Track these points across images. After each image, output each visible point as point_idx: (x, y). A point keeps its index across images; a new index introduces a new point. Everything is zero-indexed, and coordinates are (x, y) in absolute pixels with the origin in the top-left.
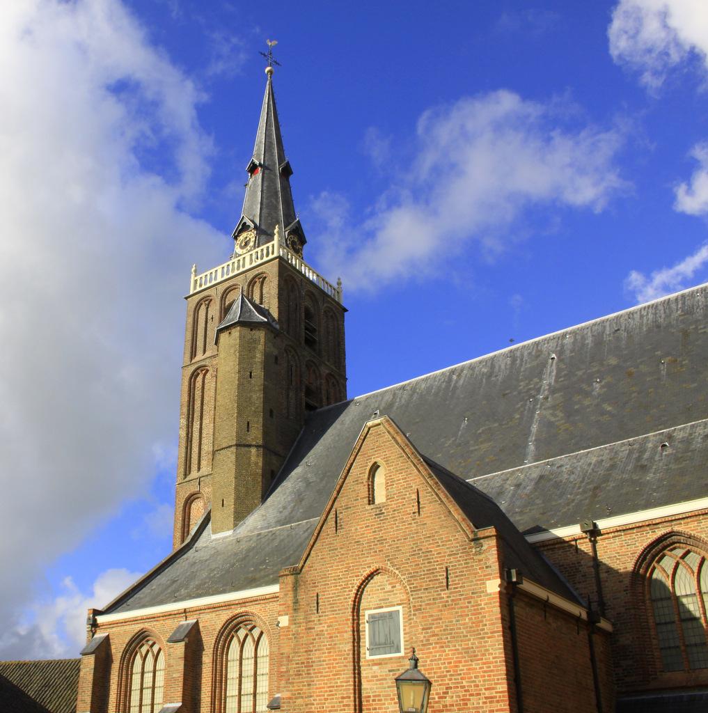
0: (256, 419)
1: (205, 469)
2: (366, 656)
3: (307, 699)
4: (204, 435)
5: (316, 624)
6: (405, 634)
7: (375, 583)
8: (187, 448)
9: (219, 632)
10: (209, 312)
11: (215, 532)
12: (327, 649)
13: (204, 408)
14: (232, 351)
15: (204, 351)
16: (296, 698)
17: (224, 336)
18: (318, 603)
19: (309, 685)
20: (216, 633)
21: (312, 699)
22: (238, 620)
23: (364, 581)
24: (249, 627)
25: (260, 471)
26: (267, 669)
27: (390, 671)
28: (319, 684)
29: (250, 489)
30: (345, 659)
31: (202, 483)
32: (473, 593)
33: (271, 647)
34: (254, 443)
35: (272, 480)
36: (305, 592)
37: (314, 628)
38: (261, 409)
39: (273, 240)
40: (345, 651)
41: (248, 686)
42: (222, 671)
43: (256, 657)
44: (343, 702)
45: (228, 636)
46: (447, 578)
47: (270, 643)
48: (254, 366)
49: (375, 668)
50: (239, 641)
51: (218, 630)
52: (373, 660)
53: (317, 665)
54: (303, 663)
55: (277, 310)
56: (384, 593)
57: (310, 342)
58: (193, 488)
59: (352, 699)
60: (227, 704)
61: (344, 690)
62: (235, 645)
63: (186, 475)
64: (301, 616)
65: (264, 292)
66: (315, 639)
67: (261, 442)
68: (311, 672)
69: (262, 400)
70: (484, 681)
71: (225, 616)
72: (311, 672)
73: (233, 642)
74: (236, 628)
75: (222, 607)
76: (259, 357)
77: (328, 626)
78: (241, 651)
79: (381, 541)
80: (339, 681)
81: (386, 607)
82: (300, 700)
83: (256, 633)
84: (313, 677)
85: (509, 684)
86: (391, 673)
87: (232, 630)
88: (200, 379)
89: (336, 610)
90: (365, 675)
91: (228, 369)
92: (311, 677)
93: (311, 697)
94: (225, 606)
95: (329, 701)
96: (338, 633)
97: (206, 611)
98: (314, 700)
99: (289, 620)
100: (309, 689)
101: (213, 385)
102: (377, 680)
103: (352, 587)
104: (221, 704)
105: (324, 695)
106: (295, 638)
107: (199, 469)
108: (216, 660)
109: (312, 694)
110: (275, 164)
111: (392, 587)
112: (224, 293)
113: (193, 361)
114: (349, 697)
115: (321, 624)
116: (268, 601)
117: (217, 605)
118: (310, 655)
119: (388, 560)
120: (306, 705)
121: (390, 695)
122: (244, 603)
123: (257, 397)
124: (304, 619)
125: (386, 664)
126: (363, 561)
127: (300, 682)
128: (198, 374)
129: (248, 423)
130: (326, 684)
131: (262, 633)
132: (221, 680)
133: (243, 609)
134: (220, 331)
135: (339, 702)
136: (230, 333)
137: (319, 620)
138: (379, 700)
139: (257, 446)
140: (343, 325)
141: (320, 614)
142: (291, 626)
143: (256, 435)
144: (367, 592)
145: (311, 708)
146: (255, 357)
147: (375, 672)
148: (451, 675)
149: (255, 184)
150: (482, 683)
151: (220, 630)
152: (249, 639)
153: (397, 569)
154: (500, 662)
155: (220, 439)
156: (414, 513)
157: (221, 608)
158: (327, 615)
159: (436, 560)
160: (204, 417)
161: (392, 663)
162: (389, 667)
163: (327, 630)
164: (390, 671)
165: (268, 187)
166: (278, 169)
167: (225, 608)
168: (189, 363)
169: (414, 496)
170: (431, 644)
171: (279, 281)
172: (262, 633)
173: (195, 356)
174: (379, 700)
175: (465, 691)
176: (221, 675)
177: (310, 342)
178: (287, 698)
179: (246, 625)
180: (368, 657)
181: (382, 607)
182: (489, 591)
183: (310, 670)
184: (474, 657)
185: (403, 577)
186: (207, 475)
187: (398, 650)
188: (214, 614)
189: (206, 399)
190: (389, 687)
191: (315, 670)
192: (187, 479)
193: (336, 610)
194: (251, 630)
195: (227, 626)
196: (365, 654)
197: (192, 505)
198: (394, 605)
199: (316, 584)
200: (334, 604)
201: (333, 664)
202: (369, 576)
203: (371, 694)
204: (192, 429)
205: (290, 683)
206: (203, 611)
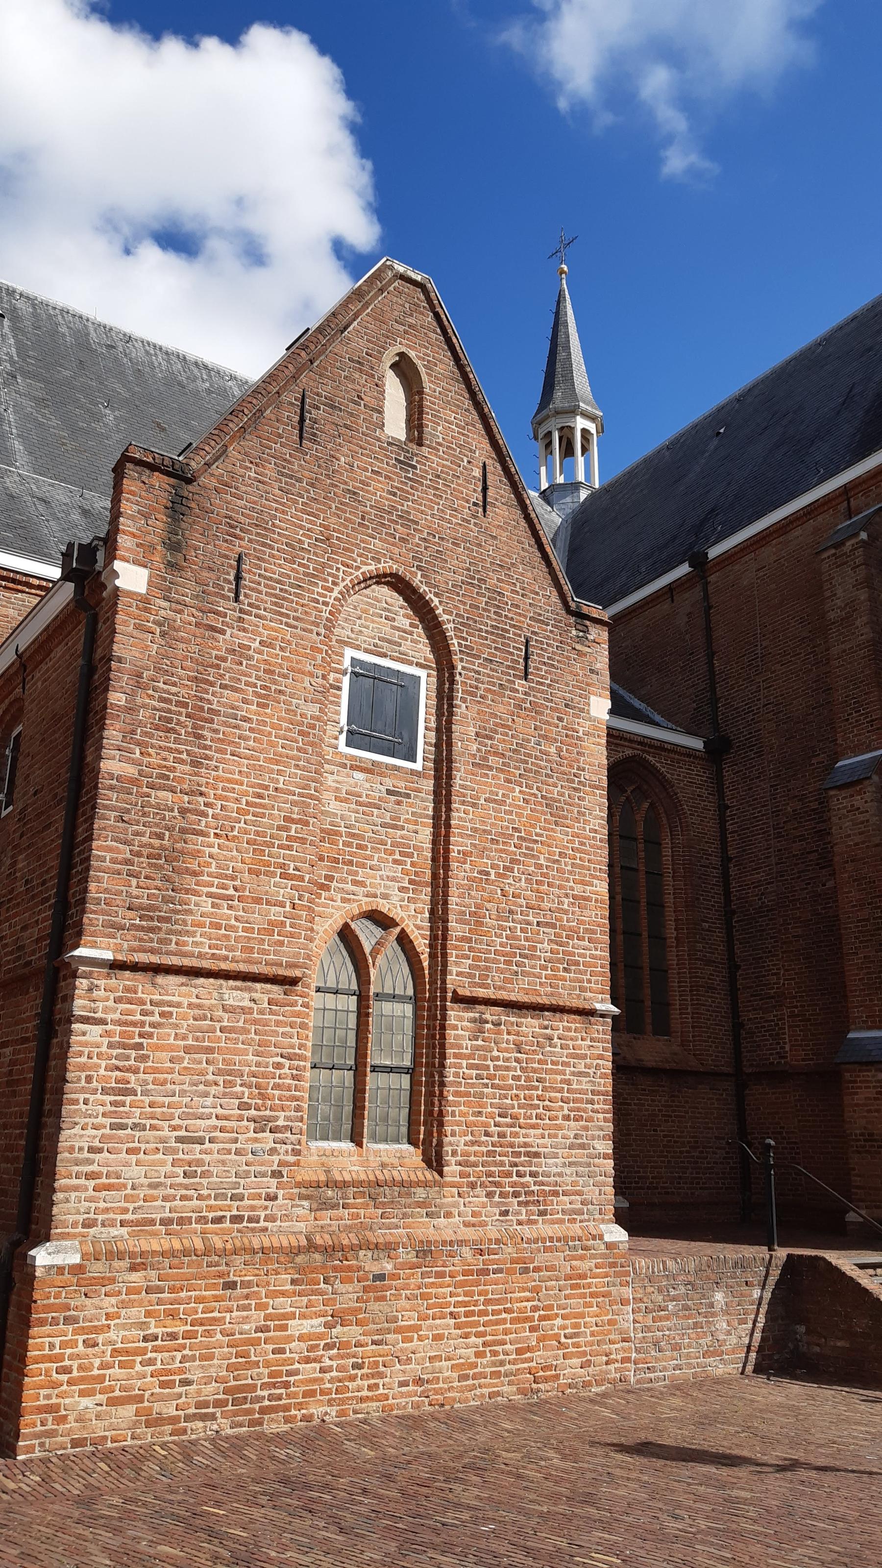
19: (195, 764)
32: (567, 706)
44: (288, 829)
46: (526, 659)
49: (359, 776)
53: (225, 724)
54: (185, 705)
64: (188, 591)
70: (573, 865)
81: (366, 651)
82: (162, 794)
84: (210, 748)
85: (24, 1347)
86: (393, 798)
102: (359, 804)
126: (362, 541)
135: (279, 828)
138: (360, 847)
148: (520, 838)
150: (569, 868)
153: (436, 595)
154: (79, 1080)
156: (475, 504)
159: (510, 615)
162: (389, 783)
164: (389, 792)
169: (477, 473)
170: (490, 768)
174: (360, 847)
175: (542, 875)
181: (384, 656)
182: (594, 713)
183: (202, 728)
184: (559, 819)
187: (412, 758)
191: (216, 731)
193: (288, 616)
198: (410, 663)
203: (343, 829)
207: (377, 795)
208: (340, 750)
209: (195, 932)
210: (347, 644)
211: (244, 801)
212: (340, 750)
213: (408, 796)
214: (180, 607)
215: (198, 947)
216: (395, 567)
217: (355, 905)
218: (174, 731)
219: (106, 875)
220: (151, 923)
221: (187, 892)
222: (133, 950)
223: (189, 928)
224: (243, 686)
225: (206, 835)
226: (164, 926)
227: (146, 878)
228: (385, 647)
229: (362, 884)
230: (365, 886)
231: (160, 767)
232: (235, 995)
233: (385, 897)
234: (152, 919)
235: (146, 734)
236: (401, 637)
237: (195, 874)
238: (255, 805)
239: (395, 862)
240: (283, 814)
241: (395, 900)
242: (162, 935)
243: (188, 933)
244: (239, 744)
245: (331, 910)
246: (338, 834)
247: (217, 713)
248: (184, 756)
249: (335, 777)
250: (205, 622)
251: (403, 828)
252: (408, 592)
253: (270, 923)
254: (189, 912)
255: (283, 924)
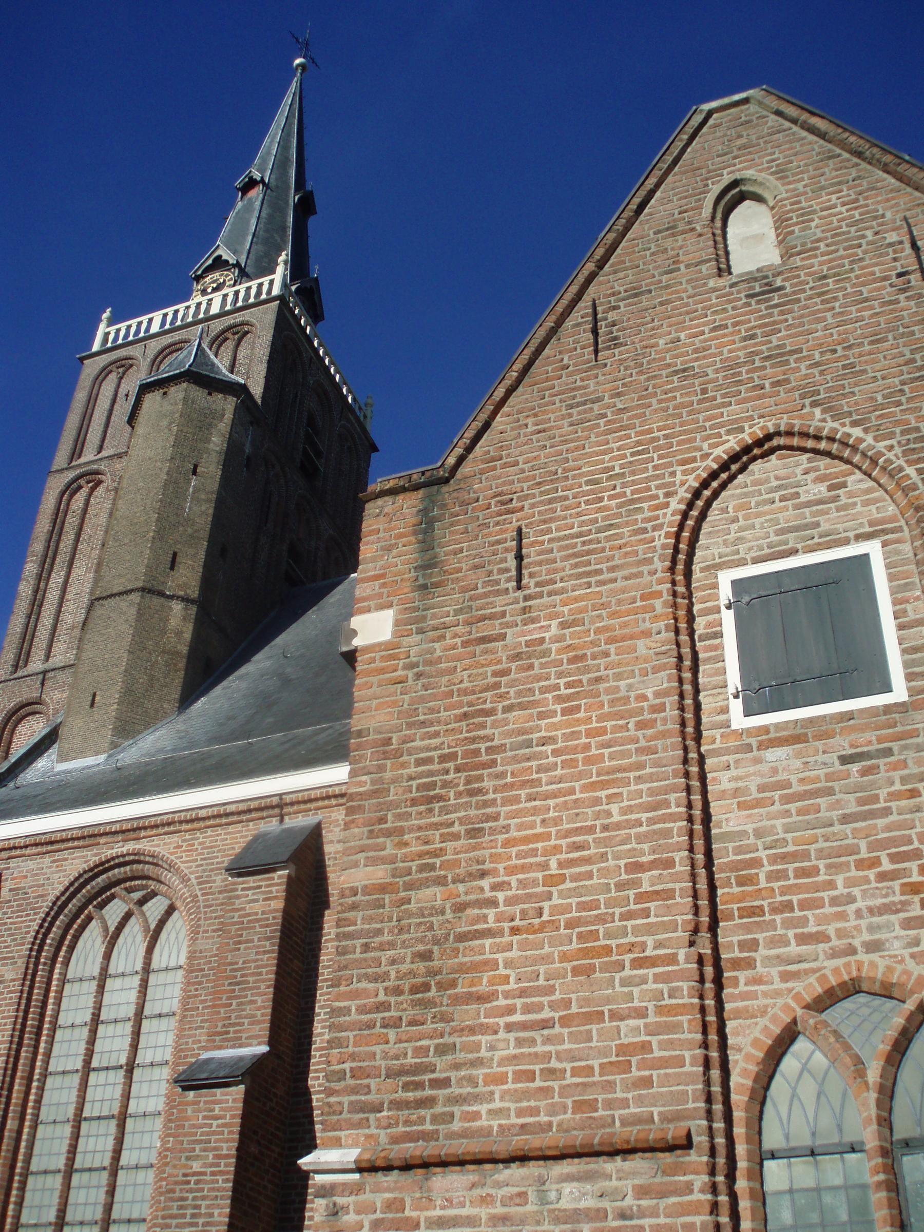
0: (191, 551)
1: (62, 654)
2: (731, 713)
3: (461, 888)
4: (69, 596)
5: (508, 625)
6: (901, 627)
7: (756, 483)
8: (29, 617)
9: (54, 903)
10: (122, 385)
11: (62, 758)
12: (559, 699)
13: (80, 547)
14: (165, 423)
15: (101, 449)
16: (409, 887)
17: (152, 401)
18: (519, 557)
19: (474, 833)
20: (45, 905)
21: (485, 883)
22: (110, 874)
23: (714, 475)
24: (137, 895)
25: (184, 649)
26: (176, 1001)
27: (845, 760)
28: (520, 827)
29: (158, 680)
30: (640, 726)
31: (48, 684)
33: (194, 940)
34: (182, 593)
35: (205, 669)
36: (466, 531)
37: (503, 637)
38: (205, 534)
39: (274, 272)
40: (644, 698)
41: (113, 1044)
42: (44, 1003)
43: (147, 969)
44: (637, 883)
45: (76, 916)
47: (195, 933)
48: (205, 456)
50: (106, 929)
51: (52, 898)
52: (765, 729)
53: (516, 760)
54: (452, 757)
55: (262, 382)
56: (796, 507)
57: (309, 470)
58: (27, 691)
59: (682, 868)
60: (46, 1094)
61: (640, 838)
62: (91, 942)
63: (16, 667)
64: (446, 606)
65: (240, 355)
66: (505, 672)
67: (194, 593)
68: (487, 784)
69: (210, 519)
71: (77, 862)
72: (487, 784)
73: (86, 934)
74: (102, 897)
75: (73, 839)
76: (217, 441)
77: (563, 625)
78: (107, 956)
79: (778, 357)
80: (614, 808)
81: (756, 561)
82: (427, 892)
83: (154, 909)
86: (855, 768)
87: (89, 901)
88: (80, 497)
89: (599, 572)
90: (726, 785)
91: (150, 453)
92: (486, 804)
93: (483, 874)
94: (83, 838)
95: (569, 885)
96: (611, 641)
97: (28, 851)
98: (494, 888)
99: (397, 623)
100: (474, 848)
101: (108, 505)
103: (667, 495)
104: (27, 1093)
105: (545, 866)
106: (419, 676)
107: (48, 657)
108: (34, 975)
109: (488, 866)
110: (289, 188)
111: (831, 488)
112: (160, 353)
113: (74, 463)
114: (670, 863)
115: (533, 621)
116: (202, 824)
117: (58, 836)
118: (483, 726)
119: (814, 404)
120: (460, 908)
121: (853, 850)
122: (134, 830)
123: (199, 510)
124: (457, 612)
125: (829, 735)
127: (436, 826)
128: (80, 487)
129: (175, 555)
130: (557, 821)
131: (171, 910)
132: (40, 1028)
133: (130, 846)
134: (145, 389)
135: (620, 886)
136: (165, 393)
137: (524, 610)
138: (802, 873)
139: (185, 600)
140: (367, 471)
141: (533, 590)
142: (406, 641)
143: (188, 577)
144: (725, 510)
145: (485, 918)
146: (208, 441)
147: (775, 771)
149: (248, 208)
151: (58, 898)
152: (134, 928)
153: (855, 424)
155: (108, 578)
157: (70, 844)
158: (563, 591)
160: (77, 563)
161: (853, 729)
162: (843, 744)
163: (559, 639)
164: (845, 760)
165: (270, 217)
166: (293, 198)
167: (81, 843)
168: (66, 466)
171: (274, 336)
172: (171, 910)
173: (79, 457)
174: (802, 873)
176: (42, 1015)
177: (309, 470)
178: (367, 890)
179: (129, 890)
180: (738, 719)
181: (794, 552)
183: (480, 779)
185: (881, 445)
186: (63, 668)
188: (47, 860)
189: (87, 530)
190: (846, 819)
192: (20, 673)
193: (599, 572)
194: (141, 902)
195: (78, 890)
196: (725, 710)
197: (20, 728)
198: (846, 542)
199: (515, 504)
200: (589, 553)
201: (587, 747)
202: (735, 457)
204: (47, 585)
205: (388, 833)
206: (18, 852)
207: (821, 773)
208: (734, 726)
209: (492, 1093)
210: (719, 567)
211: (553, 864)
212: (734, 726)
213: (889, 752)
214: (439, 632)
215: (494, 1114)
216: (770, 424)
217: (812, 979)
218: (440, 798)
219: (351, 1034)
220: (419, 1094)
221: (472, 1030)
222: (395, 1140)
223: (481, 1089)
224: (538, 696)
225: (499, 933)
226: (441, 1093)
227: (410, 1024)
228: (792, 540)
229: (821, 937)
230: (828, 939)
231: (421, 855)
232: (569, 1188)
233: (874, 947)
234: (419, 1086)
235: (399, 817)
236: (813, 514)
237: (482, 998)
238: (572, 863)
239: (883, 877)
240: (622, 863)
241: (896, 948)
242: (439, 1109)
243: (477, 1098)
244: (539, 780)
245: (762, 1001)
246: (756, 863)
247: (501, 748)
248: (456, 828)
249: (733, 772)
250: (474, 636)
251: (887, 812)
252: (756, 451)
253: (623, 1050)
254: (478, 1063)
255: (645, 1047)
